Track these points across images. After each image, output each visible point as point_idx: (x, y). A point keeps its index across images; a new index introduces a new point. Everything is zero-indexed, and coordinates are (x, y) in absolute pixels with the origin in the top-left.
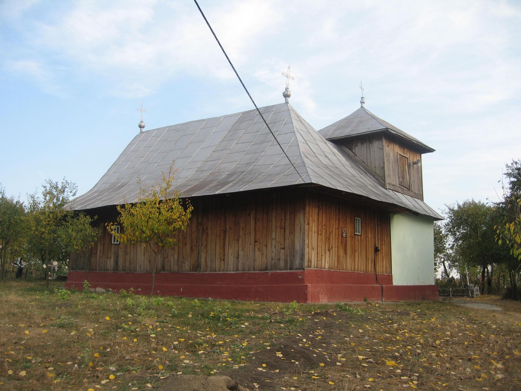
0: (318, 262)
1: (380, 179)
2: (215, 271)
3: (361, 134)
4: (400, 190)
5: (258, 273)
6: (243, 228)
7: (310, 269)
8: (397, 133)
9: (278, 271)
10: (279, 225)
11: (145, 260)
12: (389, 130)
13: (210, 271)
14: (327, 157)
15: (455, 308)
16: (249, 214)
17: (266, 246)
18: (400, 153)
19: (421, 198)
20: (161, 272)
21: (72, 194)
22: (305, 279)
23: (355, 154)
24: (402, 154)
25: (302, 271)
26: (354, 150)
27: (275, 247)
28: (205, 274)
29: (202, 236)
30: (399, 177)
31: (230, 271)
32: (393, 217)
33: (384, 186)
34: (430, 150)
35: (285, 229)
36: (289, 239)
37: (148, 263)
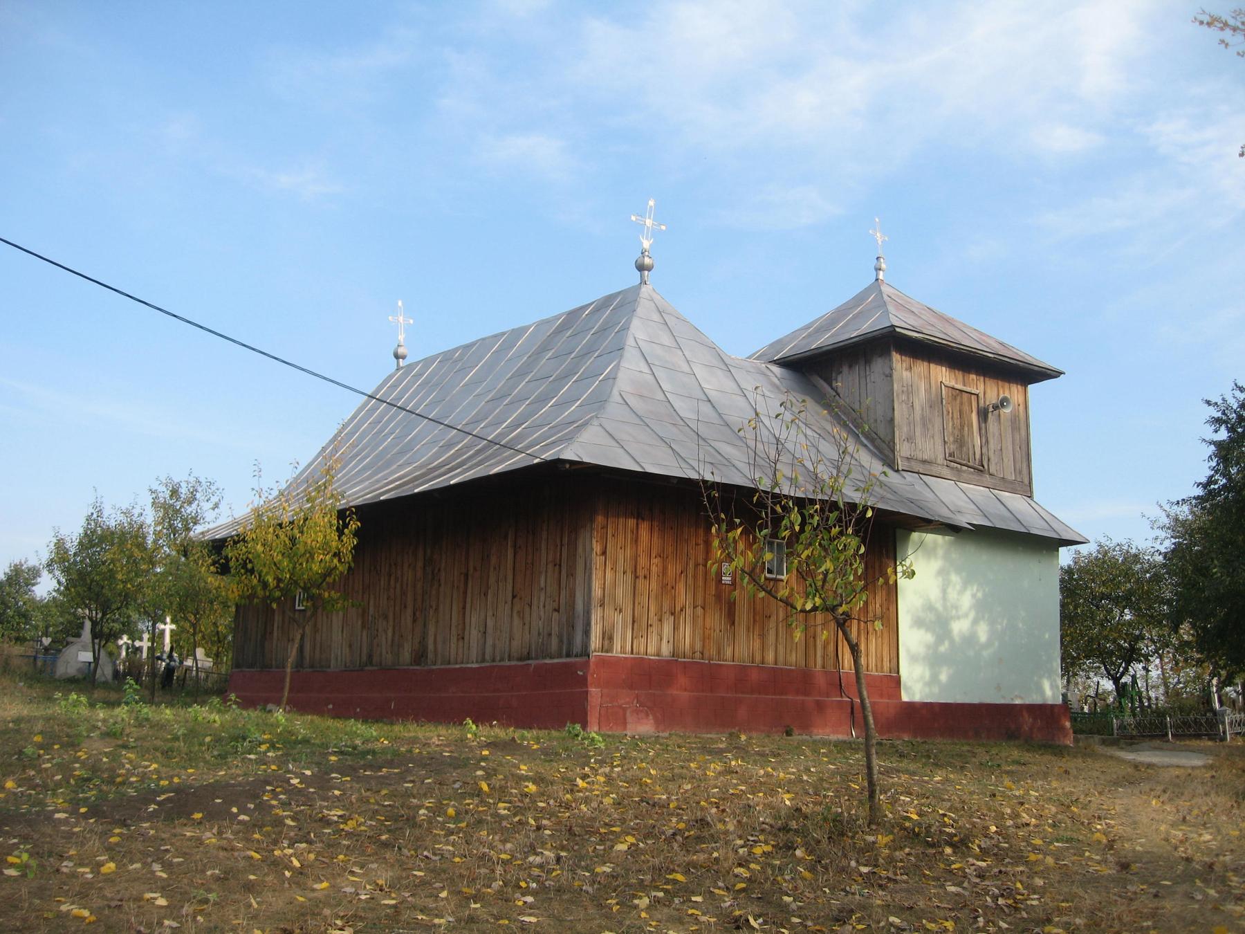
2: (449, 663)
3: (846, 343)
4: (946, 472)
5: (516, 666)
7: (610, 654)
9: (548, 661)
11: (344, 643)
12: (898, 330)
13: (441, 664)
14: (710, 401)
15: (50, 730)
16: (506, 538)
18: (953, 384)
19: (1026, 489)
20: (366, 668)
21: (210, 505)
23: (836, 392)
24: (959, 386)
25: (584, 659)
26: (834, 384)
27: (544, 607)
28: (433, 670)
30: (945, 441)
31: (473, 662)
32: (906, 538)
33: (890, 462)
34: (1064, 373)
35: (560, 565)
36: (407, 584)
37: (348, 649)
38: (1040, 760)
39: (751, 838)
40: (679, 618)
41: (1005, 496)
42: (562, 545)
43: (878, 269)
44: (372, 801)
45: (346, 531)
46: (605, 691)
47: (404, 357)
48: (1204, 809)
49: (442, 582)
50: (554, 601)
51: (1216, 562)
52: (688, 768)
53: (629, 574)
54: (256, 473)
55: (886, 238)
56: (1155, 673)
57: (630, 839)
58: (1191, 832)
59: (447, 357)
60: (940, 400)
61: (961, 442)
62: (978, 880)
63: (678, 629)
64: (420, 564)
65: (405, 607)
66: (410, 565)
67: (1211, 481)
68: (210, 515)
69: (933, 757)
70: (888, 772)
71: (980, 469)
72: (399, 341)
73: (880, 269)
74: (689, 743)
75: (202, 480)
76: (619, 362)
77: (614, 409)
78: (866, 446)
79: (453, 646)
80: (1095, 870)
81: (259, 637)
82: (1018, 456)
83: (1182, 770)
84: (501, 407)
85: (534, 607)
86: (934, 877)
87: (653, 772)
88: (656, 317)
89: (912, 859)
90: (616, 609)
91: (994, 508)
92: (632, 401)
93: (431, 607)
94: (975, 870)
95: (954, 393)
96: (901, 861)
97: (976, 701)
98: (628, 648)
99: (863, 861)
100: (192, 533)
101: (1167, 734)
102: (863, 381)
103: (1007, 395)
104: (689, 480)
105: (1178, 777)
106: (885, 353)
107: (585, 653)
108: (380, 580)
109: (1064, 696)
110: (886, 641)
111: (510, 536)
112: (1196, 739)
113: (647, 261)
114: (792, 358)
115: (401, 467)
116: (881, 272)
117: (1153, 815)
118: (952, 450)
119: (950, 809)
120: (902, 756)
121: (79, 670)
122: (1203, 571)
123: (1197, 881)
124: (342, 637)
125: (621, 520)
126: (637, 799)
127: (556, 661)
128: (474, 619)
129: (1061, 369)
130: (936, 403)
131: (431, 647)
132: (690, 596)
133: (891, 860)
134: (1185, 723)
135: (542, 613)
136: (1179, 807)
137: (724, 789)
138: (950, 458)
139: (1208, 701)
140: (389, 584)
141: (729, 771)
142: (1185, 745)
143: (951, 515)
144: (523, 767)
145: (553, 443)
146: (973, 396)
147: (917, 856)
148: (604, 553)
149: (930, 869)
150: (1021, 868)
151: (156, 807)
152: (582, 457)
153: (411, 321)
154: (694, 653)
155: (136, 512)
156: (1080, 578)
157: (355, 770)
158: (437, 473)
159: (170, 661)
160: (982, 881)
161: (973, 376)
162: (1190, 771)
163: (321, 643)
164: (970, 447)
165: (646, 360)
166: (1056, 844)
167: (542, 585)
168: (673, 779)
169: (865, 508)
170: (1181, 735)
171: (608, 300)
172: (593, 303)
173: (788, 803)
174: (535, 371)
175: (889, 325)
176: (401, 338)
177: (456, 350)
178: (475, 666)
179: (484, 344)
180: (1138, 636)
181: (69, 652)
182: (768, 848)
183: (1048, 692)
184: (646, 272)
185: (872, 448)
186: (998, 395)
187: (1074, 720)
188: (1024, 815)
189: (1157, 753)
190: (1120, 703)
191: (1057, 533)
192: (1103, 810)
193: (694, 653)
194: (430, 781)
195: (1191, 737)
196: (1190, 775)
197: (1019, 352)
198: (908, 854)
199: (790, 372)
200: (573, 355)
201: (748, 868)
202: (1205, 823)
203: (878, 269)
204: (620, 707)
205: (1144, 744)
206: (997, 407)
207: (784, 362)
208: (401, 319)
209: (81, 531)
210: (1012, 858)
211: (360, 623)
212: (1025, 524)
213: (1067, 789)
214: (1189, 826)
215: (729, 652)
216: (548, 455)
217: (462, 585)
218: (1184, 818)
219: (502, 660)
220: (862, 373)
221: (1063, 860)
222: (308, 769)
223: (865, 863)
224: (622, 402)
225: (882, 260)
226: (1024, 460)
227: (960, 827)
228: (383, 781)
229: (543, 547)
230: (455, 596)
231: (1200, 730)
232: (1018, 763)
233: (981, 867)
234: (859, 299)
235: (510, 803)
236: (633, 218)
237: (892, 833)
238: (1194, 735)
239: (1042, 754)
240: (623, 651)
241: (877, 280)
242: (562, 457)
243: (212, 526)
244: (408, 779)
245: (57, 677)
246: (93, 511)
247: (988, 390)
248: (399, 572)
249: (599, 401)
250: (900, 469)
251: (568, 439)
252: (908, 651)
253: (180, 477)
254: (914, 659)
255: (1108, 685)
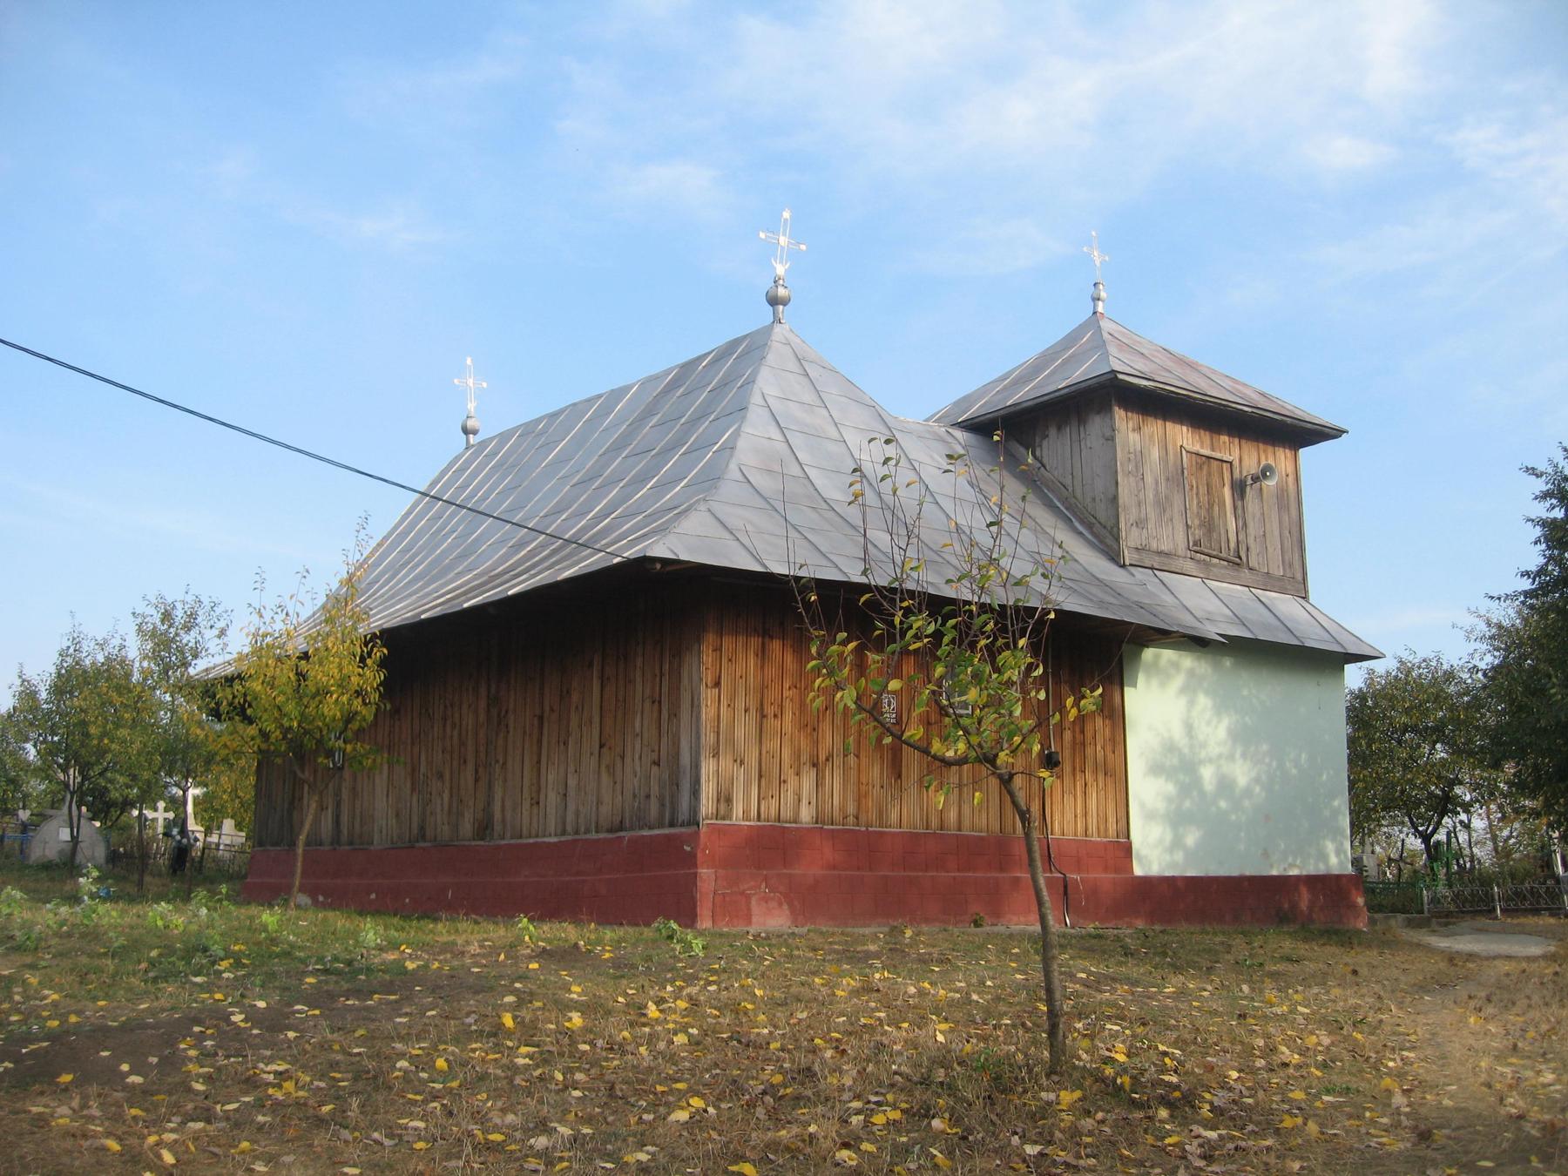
0: (763, 803)
1: (1108, 534)
2: (521, 837)
3: (1052, 396)
4: (1189, 566)
5: (605, 839)
6: (577, 707)
7: (728, 822)
8: (1161, 386)
9: (645, 833)
10: (648, 692)
12: (1121, 376)
13: (512, 838)
16: (591, 665)
17: (623, 758)
18: (1197, 448)
19: (1299, 588)
20: (417, 845)
21: (216, 632)
22: (699, 855)
24: (1206, 452)
25: (693, 829)
29: (497, 735)
30: (1187, 525)
31: (550, 835)
32: (1136, 656)
33: (1115, 557)
35: (660, 702)
37: (394, 821)
38: (1318, 955)
39: (874, 1099)
40: (824, 771)
41: (1270, 596)
42: (662, 675)
43: (1096, 299)
44: (336, 1047)
45: (369, 661)
46: (721, 872)
47: (475, 432)
48: (1544, 1027)
49: (511, 725)
50: (653, 751)
51: (1554, 680)
52: (810, 986)
53: (753, 712)
54: (257, 585)
55: (1107, 258)
56: (1478, 824)
57: (697, 1102)
58: (1525, 1067)
59: (528, 430)
60: (1180, 471)
61: (1209, 526)
62: (1202, 1163)
63: (823, 785)
64: (483, 704)
65: (465, 762)
66: (470, 706)
67: (1541, 571)
68: (213, 645)
69: (1170, 953)
70: (1095, 984)
71: (1237, 562)
72: (470, 412)
73: (1099, 299)
74: (831, 943)
75: (206, 601)
76: (740, 427)
77: (730, 489)
78: (1080, 533)
79: (526, 813)
80: (1379, 1144)
81: (286, 806)
82: (1287, 544)
83: (1514, 964)
84: (589, 492)
85: (628, 760)
86: (1135, 1160)
87: (759, 992)
88: (792, 365)
89: (1106, 1129)
90: (735, 761)
91: (1255, 614)
92: (756, 479)
93: (497, 761)
94: (1201, 1146)
95: (1199, 461)
96: (1090, 1134)
97: (1235, 873)
98: (754, 813)
99: (1032, 1134)
100: (192, 671)
101: (1494, 909)
102: (1076, 449)
103: (1271, 461)
104: (769, 577)
105: (1507, 975)
106: (1104, 408)
107: (694, 821)
108: (433, 727)
109: (1356, 862)
110: (1111, 796)
111: (595, 663)
112: (1534, 915)
113: (781, 292)
114: (982, 418)
115: (460, 575)
116: (1100, 303)
117: (1471, 1041)
118: (1197, 537)
119: (1175, 1044)
120: (1128, 953)
121: (61, 852)
122: (1539, 692)
123: (1533, 1158)
124: (387, 801)
125: (741, 639)
126: (725, 1036)
127: (656, 832)
128: (551, 777)
129: (1343, 426)
130: (1177, 478)
131: (498, 815)
132: (838, 739)
133: (1074, 1133)
134: (1516, 894)
135: (638, 769)
136: (1509, 1026)
137: (852, 1018)
138: (1195, 548)
139: (1548, 864)
140: (444, 731)
141: (868, 989)
142: (1518, 924)
143: (1197, 624)
144: (576, 989)
145: (644, 535)
146: (1224, 465)
147: (1115, 1126)
148: (717, 684)
149: (1130, 1146)
150: (1269, 1142)
151: (11, 1065)
152: (678, 553)
153: (485, 385)
154: (845, 817)
155: (116, 642)
156: (1376, 705)
157: (332, 996)
158: (498, 581)
159: (182, 838)
160: (1208, 1166)
161: (1224, 438)
162: (1524, 965)
163: (361, 813)
164: (1222, 532)
165: (778, 423)
166: (1326, 1098)
167: (638, 730)
168: (784, 1004)
169: (1046, 612)
170: (1513, 910)
171: (736, 343)
172: (709, 353)
173: (940, 1038)
174: (635, 443)
175: (1108, 370)
176: (471, 406)
177: (539, 421)
178: (554, 840)
179: (576, 409)
180: (1453, 780)
181: (48, 829)
182: (895, 1115)
183: (1333, 860)
184: (781, 307)
185: (1090, 537)
186: (1259, 462)
187: (1370, 891)
188: (1284, 1049)
189: (1482, 937)
190: (1432, 869)
191: (1342, 646)
192: (1400, 1034)
193: (845, 817)
194: (434, 1013)
195: (1526, 912)
196: (1524, 971)
197: (1285, 405)
198: (1102, 1122)
199: (979, 437)
200: (683, 420)
201: (858, 1150)
202: (1545, 1054)
203: (1096, 299)
204: (742, 893)
205: (1464, 924)
206: (1258, 478)
207: (971, 425)
208: (471, 382)
209: (53, 670)
210: (1258, 1124)
211: (409, 785)
212: (1298, 635)
213: (1352, 1001)
214: (1523, 1058)
215: (894, 816)
216: (630, 554)
217: (536, 731)
218: (1515, 1046)
219: (587, 831)
220: (1075, 436)
221: (1333, 1127)
222: (261, 998)
223: (1034, 1138)
224: (742, 479)
225: (1101, 287)
226: (1296, 549)
227: (1186, 1073)
228: (366, 1016)
229: (639, 679)
230: (526, 747)
231: (1538, 903)
232: (1289, 959)
233: (1209, 1141)
234: (1071, 339)
235: (538, 1046)
236: (762, 235)
237: (1080, 1087)
238: (1531, 910)
239: (1324, 945)
240: (746, 816)
241: (1095, 313)
242: (650, 553)
243: (219, 660)
244: (404, 1011)
245: (31, 863)
246: (69, 644)
247: (1245, 456)
248: (457, 715)
249: (711, 480)
250: (1127, 563)
251: (662, 530)
252: (1142, 805)
253: (174, 594)
254: (1150, 816)
255: (1415, 843)
